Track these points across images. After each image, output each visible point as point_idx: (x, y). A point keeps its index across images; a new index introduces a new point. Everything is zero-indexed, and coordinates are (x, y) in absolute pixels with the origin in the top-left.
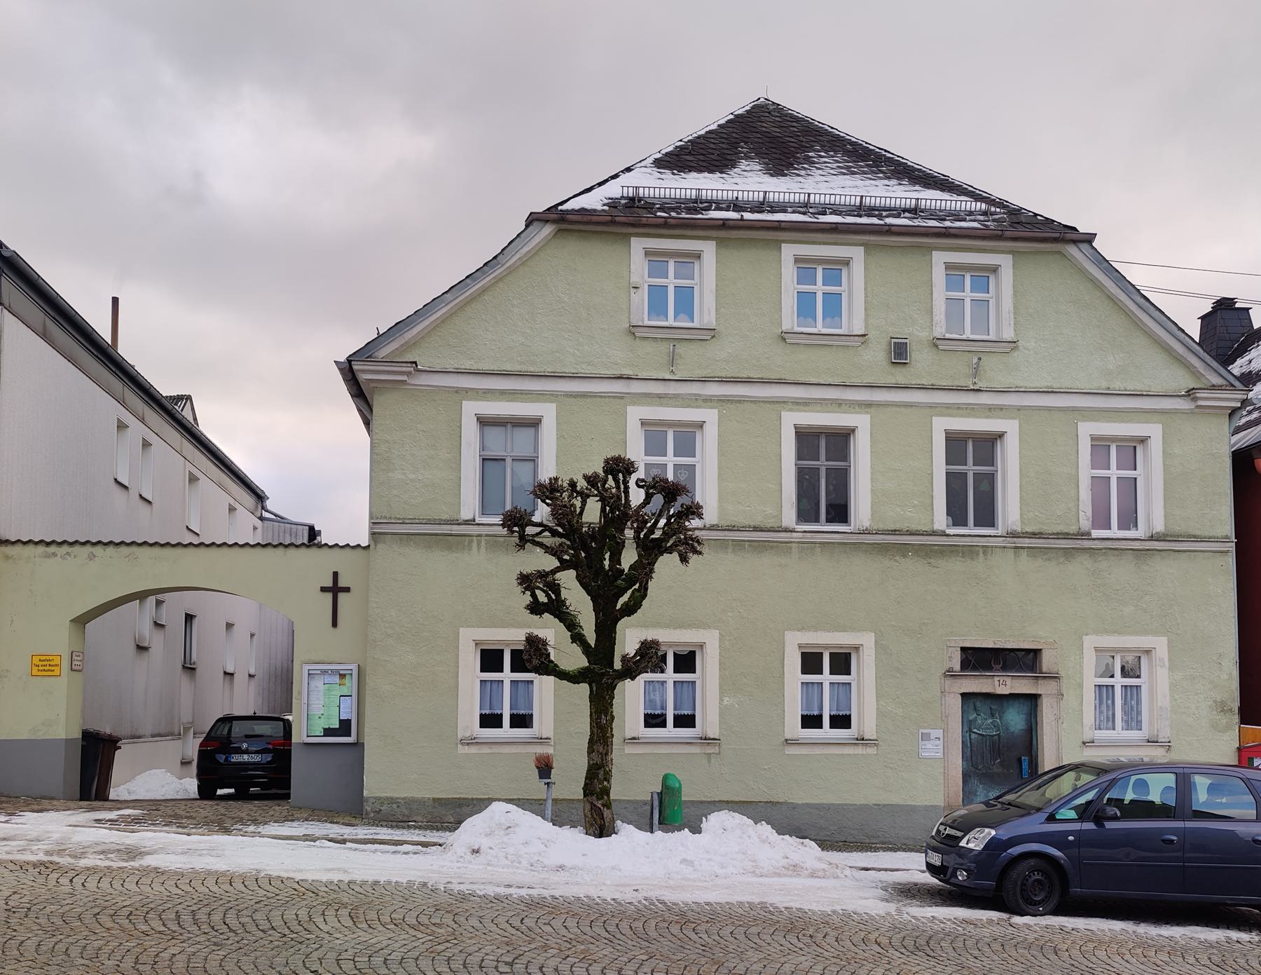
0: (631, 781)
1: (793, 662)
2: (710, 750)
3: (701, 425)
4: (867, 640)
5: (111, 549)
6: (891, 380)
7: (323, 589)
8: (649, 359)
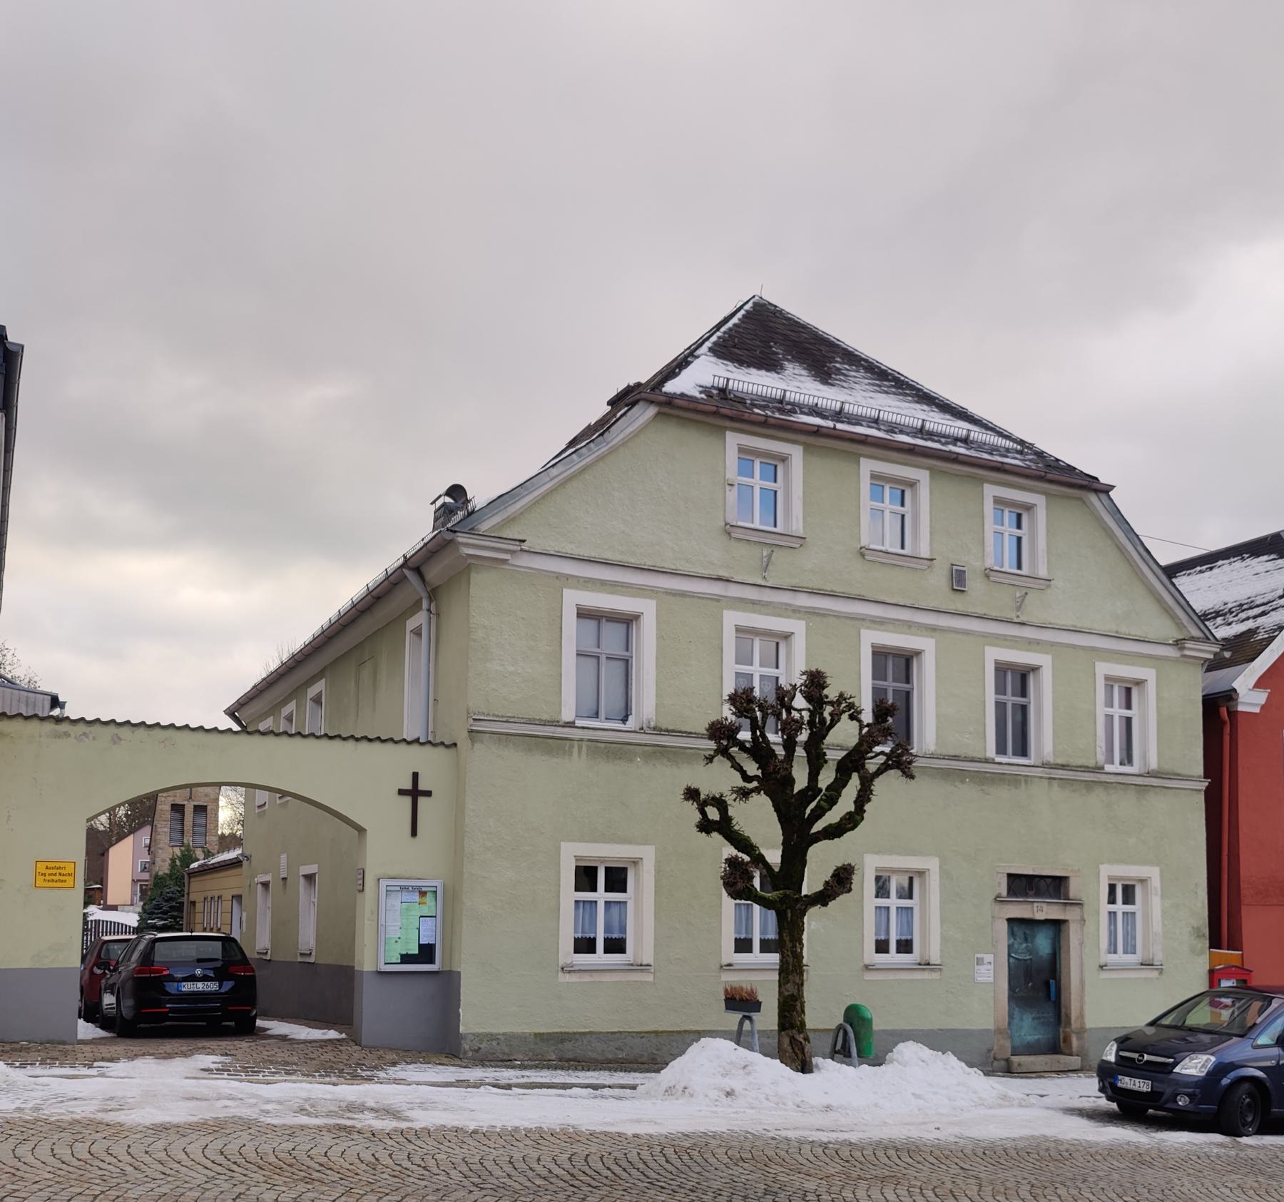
1: (568, 877)
4: (647, 854)
7: (402, 792)
8: (743, 561)
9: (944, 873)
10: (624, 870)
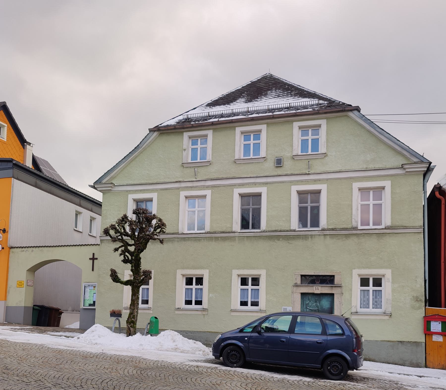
0: (142, 322)
2: (204, 313)
3: (383, 188)
5: (37, 248)
6: (276, 173)
7: (90, 259)
8: (188, 174)
9: (268, 275)
10: (381, 279)
